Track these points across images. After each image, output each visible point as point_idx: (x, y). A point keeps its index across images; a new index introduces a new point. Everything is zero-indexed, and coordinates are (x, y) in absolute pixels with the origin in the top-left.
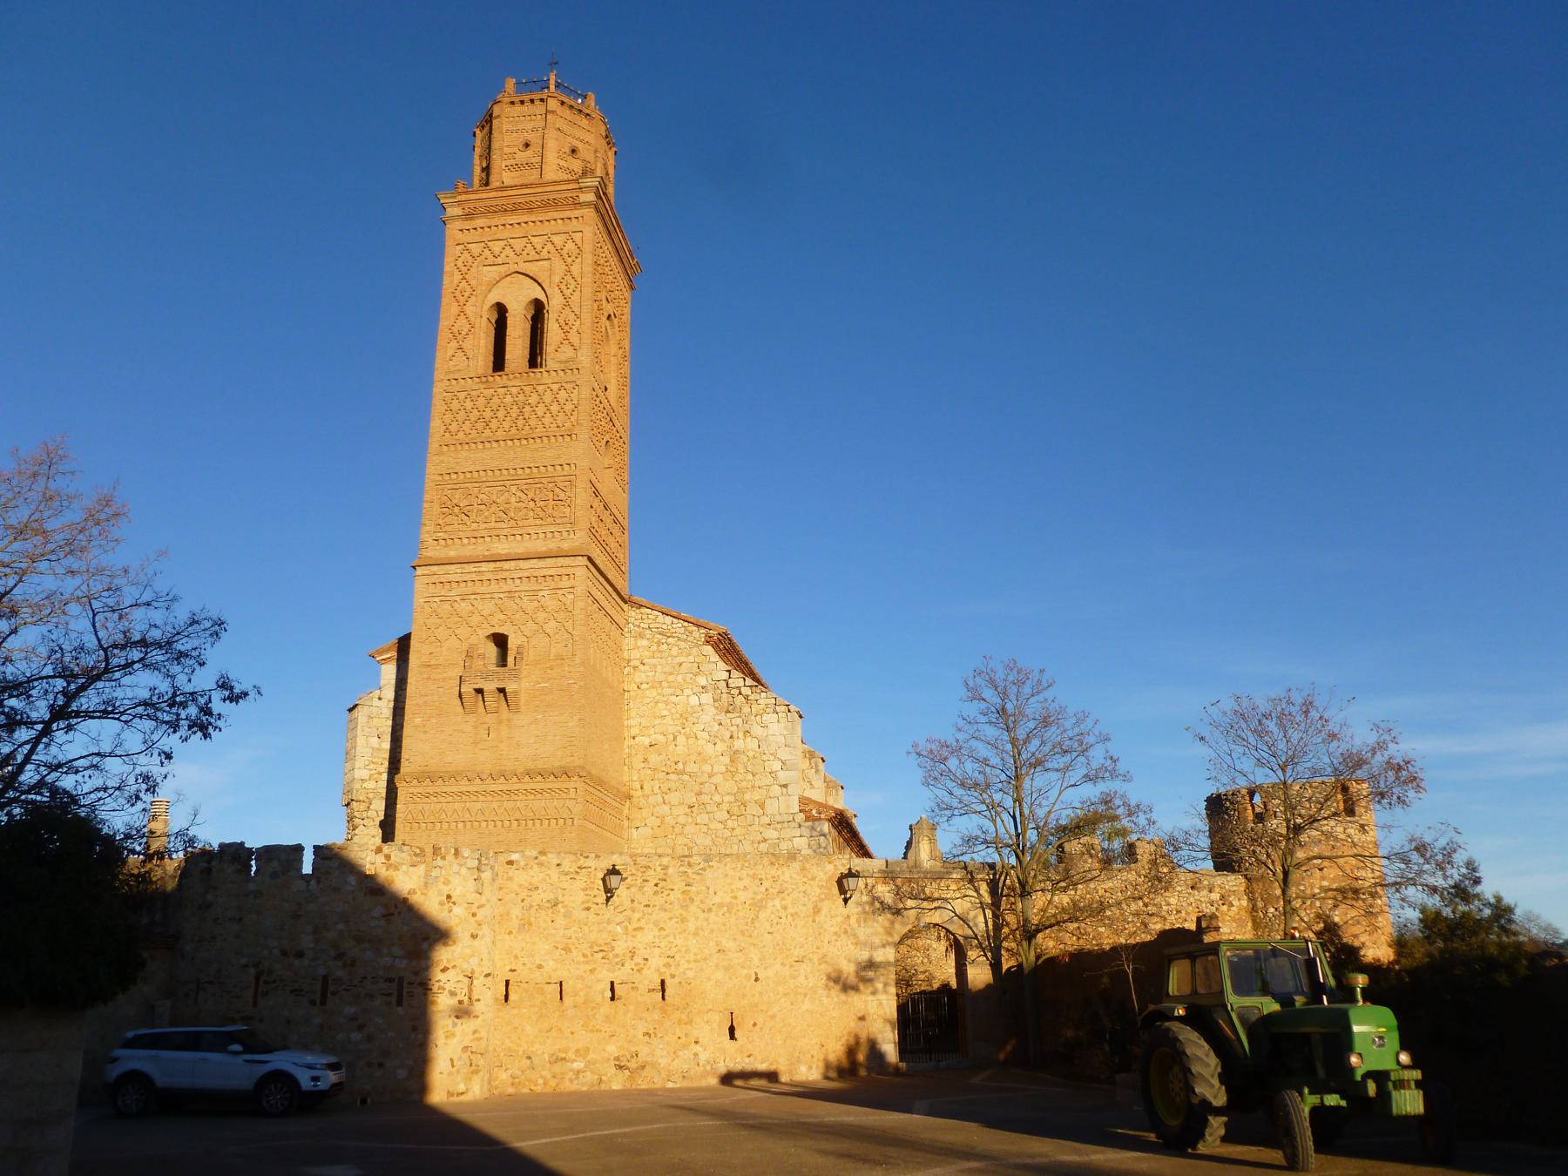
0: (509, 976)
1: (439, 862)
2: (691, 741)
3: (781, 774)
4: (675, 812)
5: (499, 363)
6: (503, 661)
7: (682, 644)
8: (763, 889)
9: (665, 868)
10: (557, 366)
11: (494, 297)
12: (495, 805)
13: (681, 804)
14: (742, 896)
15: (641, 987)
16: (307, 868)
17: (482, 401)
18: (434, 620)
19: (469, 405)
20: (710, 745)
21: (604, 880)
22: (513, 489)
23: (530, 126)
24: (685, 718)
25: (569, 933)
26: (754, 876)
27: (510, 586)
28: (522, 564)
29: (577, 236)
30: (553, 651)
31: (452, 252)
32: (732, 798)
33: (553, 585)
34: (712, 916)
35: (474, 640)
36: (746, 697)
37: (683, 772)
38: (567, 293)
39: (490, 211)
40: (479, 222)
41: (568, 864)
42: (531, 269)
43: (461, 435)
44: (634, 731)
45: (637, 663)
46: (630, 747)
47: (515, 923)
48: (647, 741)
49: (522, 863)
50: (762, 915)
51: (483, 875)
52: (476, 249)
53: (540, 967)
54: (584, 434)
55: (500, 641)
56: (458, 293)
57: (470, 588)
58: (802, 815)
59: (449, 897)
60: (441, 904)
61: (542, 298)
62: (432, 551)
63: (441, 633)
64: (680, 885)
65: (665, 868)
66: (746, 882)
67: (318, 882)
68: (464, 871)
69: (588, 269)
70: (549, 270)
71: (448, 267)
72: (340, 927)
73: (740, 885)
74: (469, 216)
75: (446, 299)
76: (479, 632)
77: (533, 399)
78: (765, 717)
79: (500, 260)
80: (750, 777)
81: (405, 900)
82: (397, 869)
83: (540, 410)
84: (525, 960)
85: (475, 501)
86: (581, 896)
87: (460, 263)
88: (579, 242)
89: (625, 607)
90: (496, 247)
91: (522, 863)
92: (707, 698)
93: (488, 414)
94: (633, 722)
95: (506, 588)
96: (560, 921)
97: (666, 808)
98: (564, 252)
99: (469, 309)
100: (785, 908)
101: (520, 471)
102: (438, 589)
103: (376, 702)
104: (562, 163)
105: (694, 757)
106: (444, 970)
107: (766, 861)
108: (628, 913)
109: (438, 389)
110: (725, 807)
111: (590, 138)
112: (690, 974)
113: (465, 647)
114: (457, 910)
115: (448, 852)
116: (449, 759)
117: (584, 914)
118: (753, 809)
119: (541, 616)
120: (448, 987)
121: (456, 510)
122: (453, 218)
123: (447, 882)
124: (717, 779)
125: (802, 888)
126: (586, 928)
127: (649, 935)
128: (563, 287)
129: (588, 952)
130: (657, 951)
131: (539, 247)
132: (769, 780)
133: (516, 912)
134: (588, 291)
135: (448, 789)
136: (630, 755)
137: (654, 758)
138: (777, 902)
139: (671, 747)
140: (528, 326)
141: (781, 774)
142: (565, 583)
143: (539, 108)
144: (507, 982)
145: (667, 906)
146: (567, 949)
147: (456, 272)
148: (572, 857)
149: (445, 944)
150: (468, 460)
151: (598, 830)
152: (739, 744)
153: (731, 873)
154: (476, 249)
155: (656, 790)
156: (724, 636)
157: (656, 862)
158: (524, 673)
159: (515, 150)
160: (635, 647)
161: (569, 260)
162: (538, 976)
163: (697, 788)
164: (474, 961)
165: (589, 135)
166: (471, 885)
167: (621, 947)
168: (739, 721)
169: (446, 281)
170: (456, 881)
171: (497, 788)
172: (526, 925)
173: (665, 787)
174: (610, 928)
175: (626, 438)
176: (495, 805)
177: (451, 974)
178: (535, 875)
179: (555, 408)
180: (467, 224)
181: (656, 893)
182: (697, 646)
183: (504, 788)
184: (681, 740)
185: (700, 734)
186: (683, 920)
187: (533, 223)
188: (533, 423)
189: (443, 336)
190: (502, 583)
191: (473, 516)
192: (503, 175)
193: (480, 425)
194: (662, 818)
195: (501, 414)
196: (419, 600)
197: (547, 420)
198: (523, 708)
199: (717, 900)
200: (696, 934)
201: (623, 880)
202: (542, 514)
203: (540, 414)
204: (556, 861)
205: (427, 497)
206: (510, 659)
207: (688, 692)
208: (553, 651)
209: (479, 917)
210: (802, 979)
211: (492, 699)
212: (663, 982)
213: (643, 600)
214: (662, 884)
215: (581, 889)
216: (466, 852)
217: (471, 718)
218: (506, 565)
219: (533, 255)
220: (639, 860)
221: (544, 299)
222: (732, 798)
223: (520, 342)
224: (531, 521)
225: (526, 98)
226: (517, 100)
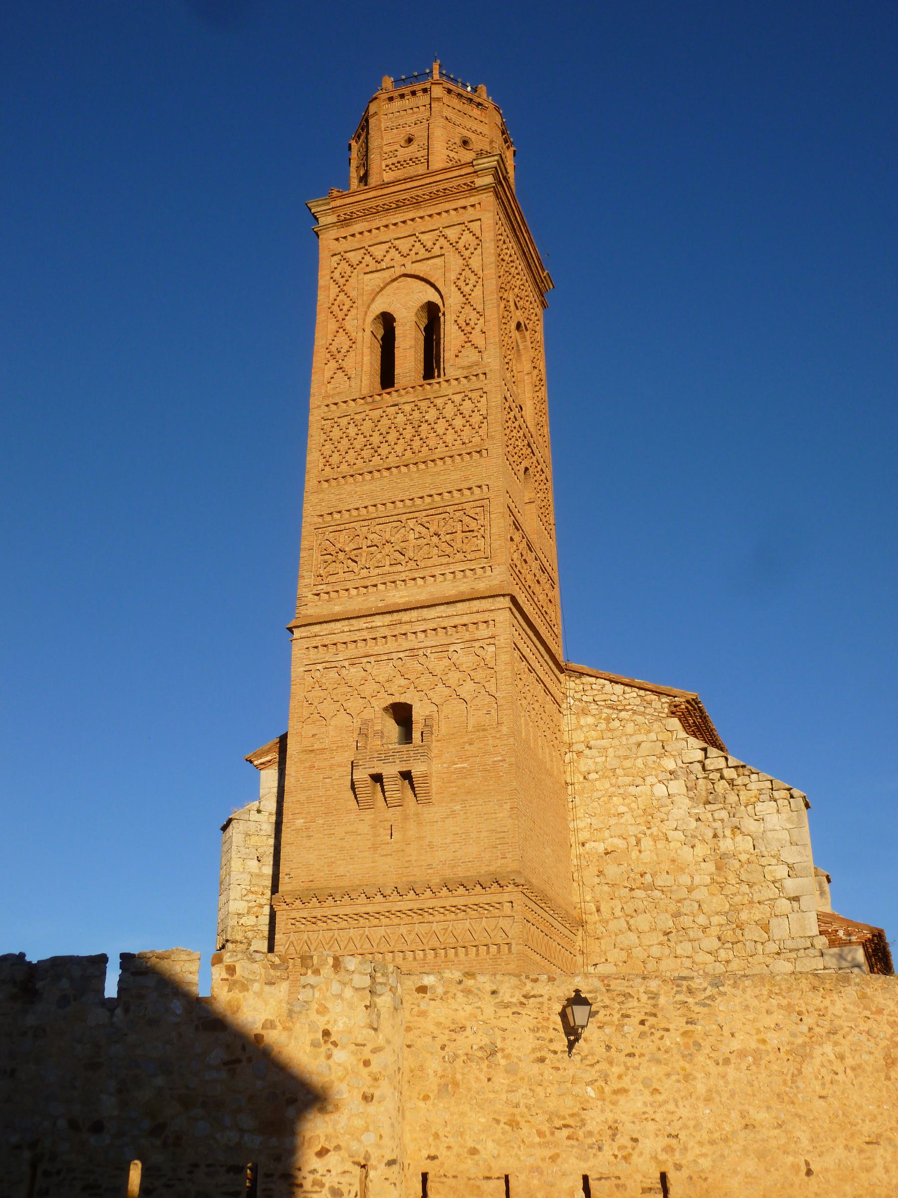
0: (427, 1166)
1: (311, 979)
2: (661, 844)
3: (789, 883)
4: (646, 942)
5: (387, 378)
6: (407, 737)
7: (640, 719)
8: (804, 1028)
9: (654, 996)
10: (459, 373)
11: (378, 307)
12: (403, 930)
13: (653, 930)
14: (774, 1040)
15: (630, 1183)
16: (111, 990)
17: (368, 424)
18: (317, 692)
19: (352, 431)
20: (687, 848)
21: (563, 1015)
22: (411, 523)
23: (413, 118)
24: (650, 813)
25: (515, 1097)
26: (789, 1008)
27: (411, 642)
28: (426, 613)
29: (475, 226)
30: (472, 722)
31: (327, 264)
32: (722, 920)
33: (467, 636)
34: (731, 1071)
35: (368, 714)
36: (731, 783)
37: (652, 887)
38: (466, 289)
39: (369, 213)
40: (357, 227)
41: (509, 992)
42: (420, 269)
43: (344, 466)
44: (584, 835)
45: (581, 747)
46: (579, 857)
47: (432, 1084)
48: (601, 847)
49: (440, 990)
50: (808, 1069)
51: (379, 1001)
52: (354, 257)
53: (474, 1152)
54: (496, 449)
55: (402, 714)
56: (335, 308)
57: (362, 648)
58: (824, 939)
59: (326, 1033)
60: (315, 1044)
61: (435, 298)
62: (311, 608)
63: (327, 708)
64: (678, 1023)
65: (654, 996)
66: (778, 1016)
67: (126, 1011)
68: (348, 993)
69: (491, 259)
70: (445, 269)
71: (324, 279)
72: (159, 1081)
73: (769, 1021)
74: (344, 222)
75: (322, 316)
76: (374, 703)
77: (431, 415)
78: (759, 807)
79: (384, 265)
80: (745, 888)
81: (259, 1038)
82: (244, 988)
83: (441, 427)
84: (451, 1141)
85: (365, 544)
86: (530, 1041)
87: (336, 275)
88: (478, 234)
89: (562, 677)
90: (378, 251)
91: (440, 990)
92: (677, 786)
93: (376, 439)
94: (581, 824)
95: (406, 645)
96: (501, 1080)
97: (633, 937)
98: (460, 245)
99: (350, 324)
100: (841, 1057)
101: (418, 502)
102: (322, 654)
103: (254, 816)
104: (452, 154)
105: (666, 866)
106: (322, 1153)
107: (804, 984)
108: (603, 1066)
109: (315, 417)
110: (714, 931)
111: (480, 128)
112: (705, 1163)
113: (357, 723)
114: (340, 1055)
115: (324, 962)
116: (341, 871)
117: (536, 1068)
118: (753, 933)
119: (454, 677)
120: (329, 1181)
121: (341, 556)
122: (327, 227)
123: (323, 1010)
124: (701, 894)
125: (864, 1027)
126: (539, 1090)
127: (636, 1102)
128: (461, 283)
129: (545, 1128)
130: (651, 1126)
131: (429, 245)
132: (773, 892)
133: (434, 1065)
134: (492, 284)
135: (340, 911)
136: (579, 868)
137: (612, 870)
138: (828, 1048)
139: (634, 854)
140: (421, 337)
141: (789, 883)
142: (483, 632)
143: (423, 99)
144: (425, 1176)
145: (661, 1055)
146: (513, 1124)
147: (333, 285)
148: (514, 981)
149: (323, 1110)
150: (354, 495)
151: (545, 963)
152: (726, 845)
153: (755, 1002)
154: (354, 257)
155: (618, 913)
156: (694, 704)
157: (639, 987)
158: (435, 751)
159: (397, 147)
160: (578, 727)
161: (467, 254)
162: (469, 1166)
163: (673, 907)
164: (369, 1139)
165: (484, 126)
166: (361, 1016)
167: (595, 1120)
168: (724, 814)
169: (321, 296)
170: (336, 1008)
171: (404, 906)
172: (449, 1086)
173: (629, 910)
174: (577, 1090)
175: (548, 473)
176: (403, 930)
177: (332, 1159)
178: (460, 1008)
179: (458, 422)
180: (343, 232)
181: (642, 1035)
182: (659, 719)
183: (415, 905)
184: (647, 843)
185: (672, 834)
186: (687, 1077)
187: (423, 228)
188: (432, 443)
189: (320, 356)
190: (401, 639)
191: (362, 561)
192: (380, 172)
193: (366, 453)
194: (629, 950)
195: (392, 437)
196: (297, 670)
197: (449, 438)
198: (435, 798)
199: (736, 1045)
200: (708, 1100)
201: (592, 1014)
202: (449, 550)
203: (440, 431)
204: (489, 987)
205: (305, 544)
206: (416, 735)
207: (650, 780)
208: (472, 722)
209: (374, 1068)
210: (879, 1172)
211: (393, 785)
212: (663, 1177)
213: (585, 668)
214: (651, 1020)
215: (529, 1032)
216: (351, 964)
217: (368, 815)
218: (405, 617)
219: (423, 254)
220: (614, 984)
221: (439, 302)
222: (722, 920)
223: (411, 354)
224: (436, 560)
225: (406, 91)
226: (396, 94)
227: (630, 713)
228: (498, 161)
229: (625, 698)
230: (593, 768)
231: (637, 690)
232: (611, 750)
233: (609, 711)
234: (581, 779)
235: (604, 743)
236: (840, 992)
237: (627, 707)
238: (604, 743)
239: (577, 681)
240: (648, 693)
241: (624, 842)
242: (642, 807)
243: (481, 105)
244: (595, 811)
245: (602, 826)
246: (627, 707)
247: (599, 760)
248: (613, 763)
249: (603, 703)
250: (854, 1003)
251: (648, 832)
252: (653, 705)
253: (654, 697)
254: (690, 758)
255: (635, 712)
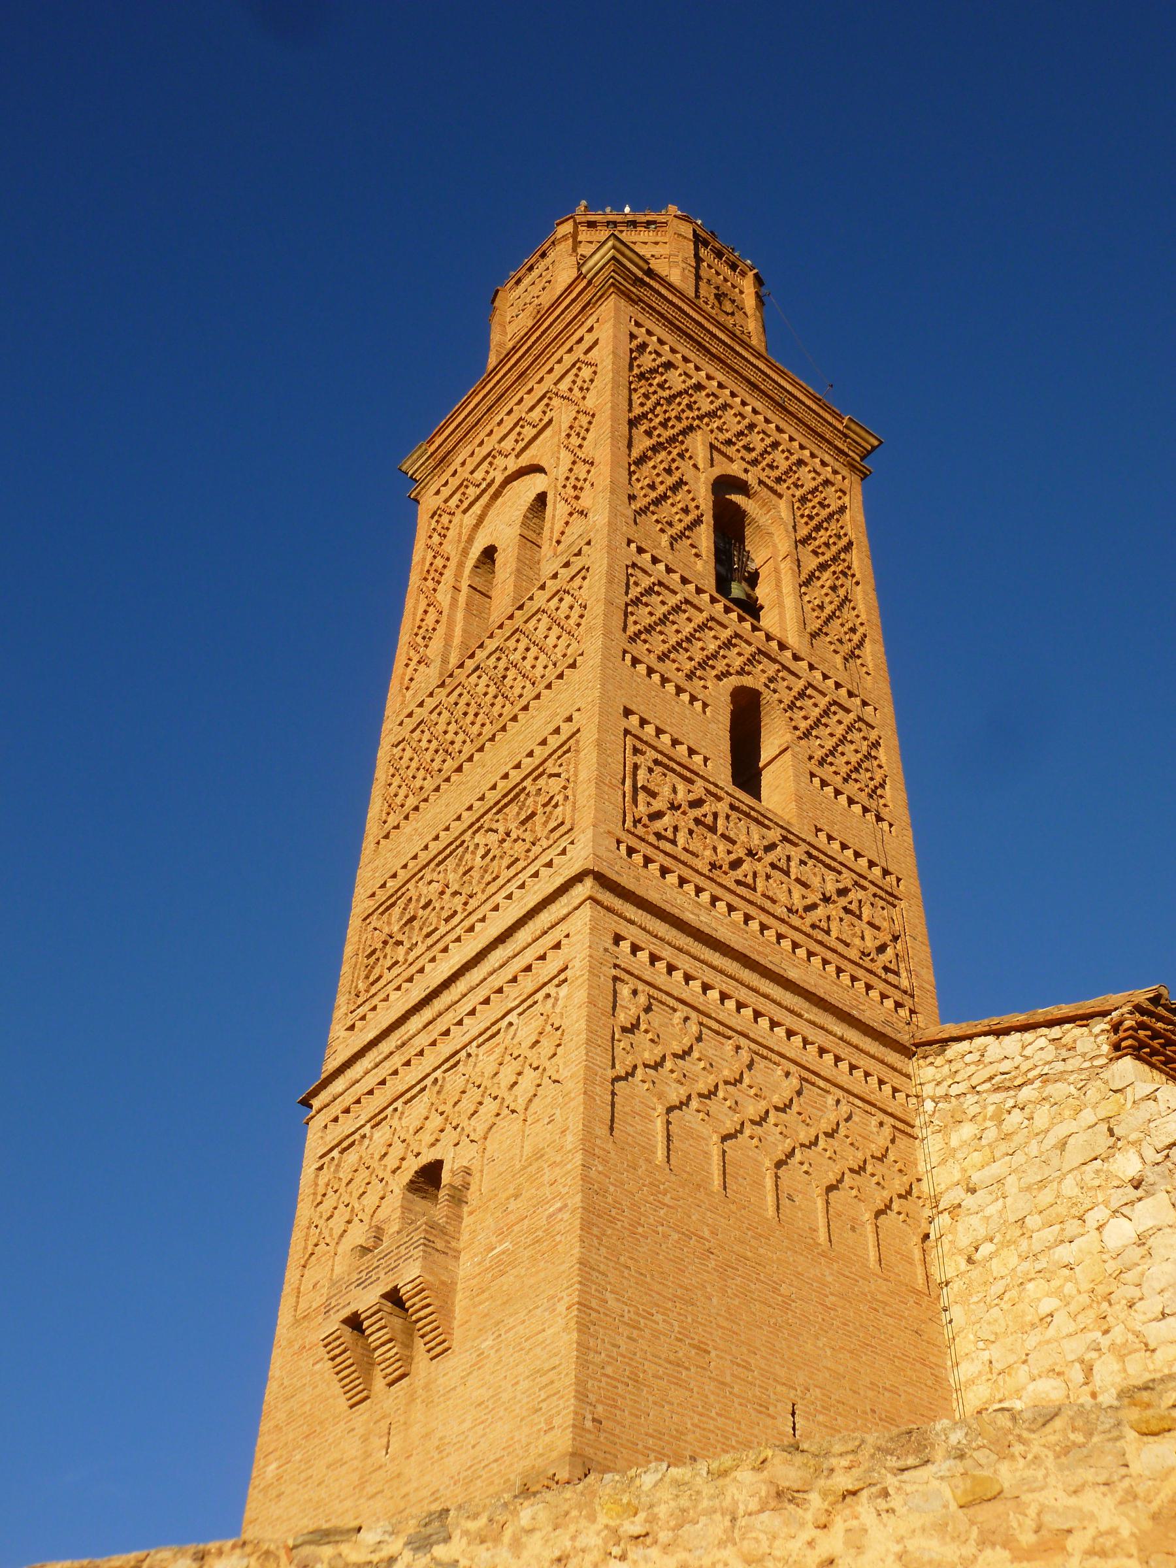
7: (1057, 1090)
89: (910, 1066)
160: (944, 1158)
227: (1037, 1084)
228: (614, 247)
229: (1027, 1058)
230: (982, 1232)
231: (1044, 1030)
232: (1011, 1180)
233: (998, 1097)
234: (963, 1266)
235: (997, 1169)
236: (885, 1494)
237: (1031, 1075)
238: (997, 1169)
239: (939, 1061)
240: (1067, 1026)
241: (1057, 1382)
242: (1085, 1286)
243: (654, 222)
244: (997, 1329)
245: (1011, 1359)
246: (1031, 1075)
247: (992, 1210)
248: (1018, 1204)
249: (987, 1086)
250: (941, 1528)
251: (1105, 1342)
252: (1080, 1048)
253: (1078, 1031)
254: (1169, 1135)
255: (1045, 1079)
